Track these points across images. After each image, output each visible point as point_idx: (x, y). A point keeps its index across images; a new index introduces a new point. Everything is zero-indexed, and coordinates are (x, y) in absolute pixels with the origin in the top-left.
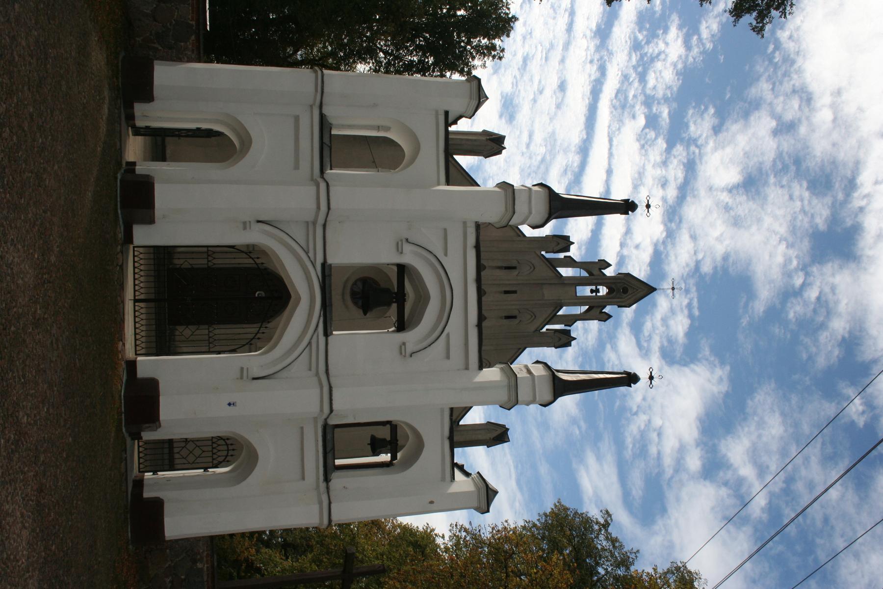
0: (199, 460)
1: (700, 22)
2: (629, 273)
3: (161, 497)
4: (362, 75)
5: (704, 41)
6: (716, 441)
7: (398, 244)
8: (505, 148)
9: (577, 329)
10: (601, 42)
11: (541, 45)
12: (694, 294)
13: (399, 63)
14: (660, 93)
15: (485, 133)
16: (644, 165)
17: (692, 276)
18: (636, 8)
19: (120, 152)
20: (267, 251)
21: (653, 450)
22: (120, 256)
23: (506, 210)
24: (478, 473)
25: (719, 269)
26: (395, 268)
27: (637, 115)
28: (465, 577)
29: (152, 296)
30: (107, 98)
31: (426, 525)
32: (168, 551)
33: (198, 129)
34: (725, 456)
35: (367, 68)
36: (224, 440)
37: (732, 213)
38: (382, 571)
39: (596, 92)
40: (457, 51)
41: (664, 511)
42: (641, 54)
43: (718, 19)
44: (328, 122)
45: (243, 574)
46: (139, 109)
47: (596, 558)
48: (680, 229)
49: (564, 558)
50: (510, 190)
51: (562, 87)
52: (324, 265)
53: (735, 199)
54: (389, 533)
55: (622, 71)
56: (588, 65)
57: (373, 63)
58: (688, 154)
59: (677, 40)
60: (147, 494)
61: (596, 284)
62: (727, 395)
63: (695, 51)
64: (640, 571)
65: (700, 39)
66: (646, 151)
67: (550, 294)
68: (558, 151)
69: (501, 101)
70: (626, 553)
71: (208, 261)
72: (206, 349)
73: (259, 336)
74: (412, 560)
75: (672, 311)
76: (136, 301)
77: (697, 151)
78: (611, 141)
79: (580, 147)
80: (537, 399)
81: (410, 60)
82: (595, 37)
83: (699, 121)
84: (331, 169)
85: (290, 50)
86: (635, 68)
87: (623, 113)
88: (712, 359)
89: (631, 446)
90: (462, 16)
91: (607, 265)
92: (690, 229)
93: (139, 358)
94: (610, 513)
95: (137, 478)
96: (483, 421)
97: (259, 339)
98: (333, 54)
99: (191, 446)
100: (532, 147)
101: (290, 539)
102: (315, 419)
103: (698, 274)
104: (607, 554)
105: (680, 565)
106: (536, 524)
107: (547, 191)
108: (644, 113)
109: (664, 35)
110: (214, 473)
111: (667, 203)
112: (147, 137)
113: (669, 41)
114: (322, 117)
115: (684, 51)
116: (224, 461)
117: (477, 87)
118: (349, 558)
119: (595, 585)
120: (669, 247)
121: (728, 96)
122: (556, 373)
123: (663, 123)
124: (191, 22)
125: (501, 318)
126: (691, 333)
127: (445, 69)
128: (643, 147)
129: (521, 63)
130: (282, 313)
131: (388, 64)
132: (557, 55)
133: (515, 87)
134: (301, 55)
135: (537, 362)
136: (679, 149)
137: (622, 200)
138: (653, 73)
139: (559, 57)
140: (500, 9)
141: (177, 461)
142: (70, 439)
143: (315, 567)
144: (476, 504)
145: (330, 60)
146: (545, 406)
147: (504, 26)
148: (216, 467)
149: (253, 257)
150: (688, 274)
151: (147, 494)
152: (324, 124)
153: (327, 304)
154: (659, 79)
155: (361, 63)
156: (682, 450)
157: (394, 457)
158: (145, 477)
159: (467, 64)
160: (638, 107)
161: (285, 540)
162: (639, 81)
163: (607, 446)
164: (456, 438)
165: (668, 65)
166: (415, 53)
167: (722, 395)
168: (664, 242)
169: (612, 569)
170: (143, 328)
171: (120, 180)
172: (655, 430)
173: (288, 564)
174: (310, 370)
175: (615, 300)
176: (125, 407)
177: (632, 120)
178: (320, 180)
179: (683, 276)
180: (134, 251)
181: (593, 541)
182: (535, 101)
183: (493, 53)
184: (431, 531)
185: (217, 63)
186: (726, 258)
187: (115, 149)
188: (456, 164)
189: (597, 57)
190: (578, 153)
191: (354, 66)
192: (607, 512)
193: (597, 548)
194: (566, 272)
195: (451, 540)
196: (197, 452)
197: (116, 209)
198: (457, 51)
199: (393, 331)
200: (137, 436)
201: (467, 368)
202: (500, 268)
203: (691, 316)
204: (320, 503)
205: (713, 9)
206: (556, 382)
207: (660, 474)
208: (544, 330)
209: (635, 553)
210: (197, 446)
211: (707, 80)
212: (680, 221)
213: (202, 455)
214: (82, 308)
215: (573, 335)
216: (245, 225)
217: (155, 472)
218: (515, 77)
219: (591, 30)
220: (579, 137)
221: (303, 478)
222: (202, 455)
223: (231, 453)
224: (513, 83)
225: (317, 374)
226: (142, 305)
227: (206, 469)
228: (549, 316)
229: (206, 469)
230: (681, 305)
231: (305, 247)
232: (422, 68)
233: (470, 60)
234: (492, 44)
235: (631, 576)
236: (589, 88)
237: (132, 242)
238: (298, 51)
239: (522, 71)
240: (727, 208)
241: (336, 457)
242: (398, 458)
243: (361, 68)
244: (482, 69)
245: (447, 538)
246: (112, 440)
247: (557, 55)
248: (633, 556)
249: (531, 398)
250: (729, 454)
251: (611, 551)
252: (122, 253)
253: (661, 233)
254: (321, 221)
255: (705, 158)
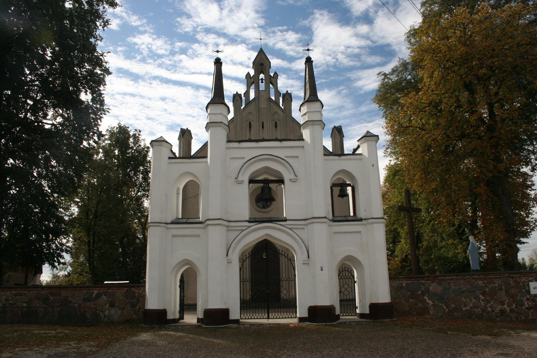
0: (350, 286)
1: (132, 26)
2: (253, 63)
3: (369, 304)
4: (150, 204)
5: (142, 23)
6: (353, 17)
7: (238, 183)
8: (187, 128)
9: (282, 90)
10: (141, 79)
11: (142, 110)
12: (276, 29)
13: (143, 185)
14: (169, 47)
15: (179, 139)
16: (206, 55)
17: (266, 29)
18: (124, 61)
19: (192, 326)
20: (242, 252)
21: (357, 51)
22: (245, 326)
23: (220, 126)
24: (358, 141)
25: (263, 15)
26: (251, 185)
27: (180, 59)
28: (412, 149)
29: (266, 310)
30: (165, 332)
31: (384, 170)
32: (396, 301)
33: (180, 286)
34: (362, 13)
35: (146, 201)
36: (340, 273)
37: (234, 8)
38: (408, 192)
39: (167, 81)
40: (137, 154)
41: (388, 45)
42: (148, 58)
43: (131, 16)
44: (175, 220)
45: (408, 264)
46: (170, 316)
47: (402, 80)
48: (241, 36)
49: (402, 97)
50: (210, 124)
51: (163, 99)
52: (249, 222)
53: (226, 7)
54: (388, 189)
55: (156, 68)
56: (153, 85)
57: (144, 198)
58: (201, 32)
59: (141, 38)
60: (367, 312)
61: (259, 80)
62: (330, 12)
63: (147, 28)
64: (409, 57)
65: (141, 26)
66: (199, 54)
67: (264, 104)
68: (198, 101)
69: (170, 131)
70: (400, 64)
71: (248, 281)
72: (293, 282)
73: (286, 255)
74: (403, 176)
75: (284, 40)
76: (268, 318)
77: (200, 27)
78: (193, 73)
79: (196, 90)
80: (319, 110)
81: (142, 178)
82: (138, 82)
83: (184, 26)
84: (200, 218)
85: (138, 241)
86: (155, 61)
87: (178, 67)
88: (310, 19)
89: (354, 63)
90: (118, 152)
91: (248, 74)
92: (241, 31)
93: (298, 316)
94: (379, 72)
95: (359, 316)
96: (331, 139)
97: (288, 255)
98: (139, 219)
99: (343, 290)
100: (195, 115)
101: (391, 240)
102: (330, 226)
103: (265, 27)
104: (400, 74)
105: (406, 36)
106: (384, 112)
107: (210, 105)
108: (179, 55)
109: (138, 45)
110: (358, 278)
111: (227, 43)
112: (185, 313)
113: (142, 42)
114: (173, 223)
115: (147, 34)
116: (351, 273)
117: (156, 142)
118: (401, 208)
119: (416, 81)
120: (250, 42)
121: (172, 11)
122: (306, 100)
123: (184, 45)
124: (125, 290)
125: (276, 130)
126: (296, 31)
127: (146, 160)
128: (197, 56)
129: (150, 121)
130: (273, 243)
131: (144, 190)
132: (147, 102)
133: (163, 124)
134: (140, 235)
135: (300, 110)
136: (199, 37)
137: (215, 66)
138: (158, 50)
139: (148, 101)
140: (114, 132)
141: (351, 297)
142: (339, 349)
143: (406, 227)
144: (374, 142)
145: (142, 220)
146: (323, 106)
147: (123, 130)
148: (354, 277)
149: (245, 258)
150: (265, 32)
151: (367, 312)
152: (175, 222)
153: (270, 220)
154: (162, 48)
155: (144, 204)
156: (357, 35)
157: (349, 185)
158: (359, 312)
159: (143, 149)
160: (176, 59)
161: (391, 243)
162: (162, 58)
163: (353, 75)
164: (339, 153)
165: (154, 43)
166: (138, 176)
167: (330, 14)
168: (247, 45)
169: (408, 72)
170: (257, 315)
171: (207, 325)
172: (346, 50)
173: (403, 241)
174: (304, 229)
175: (267, 70)
176: (323, 323)
177: (183, 61)
178: (205, 224)
179: (266, 35)
180: (243, 319)
181: (393, 82)
182: (170, 113)
183: (137, 135)
184: (388, 167)
185: (145, 278)
186: (257, 12)
187: (190, 328)
188: (196, 154)
189: (148, 81)
190: (199, 90)
191: (145, 208)
192: (378, 74)
193: (397, 79)
194: (252, 95)
195: (392, 157)
196: (346, 286)
197: (222, 327)
198: (137, 154)
199: (284, 185)
200: (338, 317)
201: (303, 147)
202: (250, 131)
203: (287, 31)
204: (373, 223)
205: (125, 19)
206: (310, 100)
207: (369, 47)
208: (283, 107)
209: (400, 59)
210: (343, 287)
211: (162, 22)
212: (237, 36)
213: (348, 284)
214: (273, 344)
215: (285, 92)
216: (229, 262)
217: (356, 308)
218: (157, 124)
219: (134, 84)
220: (190, 90)
221: (360, 232)
222: (348, 284)
223: (347, 269)
224: (161, 125)
225: (306, 225)
226: (270, 315)
227: (355, 282)
228: (276, 105)
229: (355, 282)
230: (281, 35)
231: (240, 232)
232: (146, 173)
233: (141, 147)
234: (133, 136)
235: (411, 62)
236: (165, 85)
237: (238, 320)
238: (138, 237)
239: (155, 120)
240: (231, 11)
241: (349, 215)
242: (349, 183)
243: (146, 204)
244: (146, 140)
245: (391, 159)
246: (340, 329)
247: (147, 102)
248: (401, 61)
249: (319, 113)
250: (361, 10)
251: (399, 72)
252: (244, 325)
253: (243, 46)
254: (226, 223)
255: (204, 23)
